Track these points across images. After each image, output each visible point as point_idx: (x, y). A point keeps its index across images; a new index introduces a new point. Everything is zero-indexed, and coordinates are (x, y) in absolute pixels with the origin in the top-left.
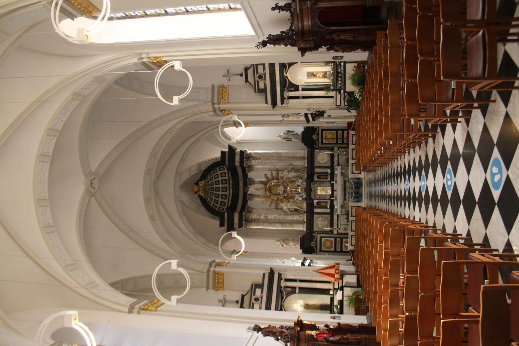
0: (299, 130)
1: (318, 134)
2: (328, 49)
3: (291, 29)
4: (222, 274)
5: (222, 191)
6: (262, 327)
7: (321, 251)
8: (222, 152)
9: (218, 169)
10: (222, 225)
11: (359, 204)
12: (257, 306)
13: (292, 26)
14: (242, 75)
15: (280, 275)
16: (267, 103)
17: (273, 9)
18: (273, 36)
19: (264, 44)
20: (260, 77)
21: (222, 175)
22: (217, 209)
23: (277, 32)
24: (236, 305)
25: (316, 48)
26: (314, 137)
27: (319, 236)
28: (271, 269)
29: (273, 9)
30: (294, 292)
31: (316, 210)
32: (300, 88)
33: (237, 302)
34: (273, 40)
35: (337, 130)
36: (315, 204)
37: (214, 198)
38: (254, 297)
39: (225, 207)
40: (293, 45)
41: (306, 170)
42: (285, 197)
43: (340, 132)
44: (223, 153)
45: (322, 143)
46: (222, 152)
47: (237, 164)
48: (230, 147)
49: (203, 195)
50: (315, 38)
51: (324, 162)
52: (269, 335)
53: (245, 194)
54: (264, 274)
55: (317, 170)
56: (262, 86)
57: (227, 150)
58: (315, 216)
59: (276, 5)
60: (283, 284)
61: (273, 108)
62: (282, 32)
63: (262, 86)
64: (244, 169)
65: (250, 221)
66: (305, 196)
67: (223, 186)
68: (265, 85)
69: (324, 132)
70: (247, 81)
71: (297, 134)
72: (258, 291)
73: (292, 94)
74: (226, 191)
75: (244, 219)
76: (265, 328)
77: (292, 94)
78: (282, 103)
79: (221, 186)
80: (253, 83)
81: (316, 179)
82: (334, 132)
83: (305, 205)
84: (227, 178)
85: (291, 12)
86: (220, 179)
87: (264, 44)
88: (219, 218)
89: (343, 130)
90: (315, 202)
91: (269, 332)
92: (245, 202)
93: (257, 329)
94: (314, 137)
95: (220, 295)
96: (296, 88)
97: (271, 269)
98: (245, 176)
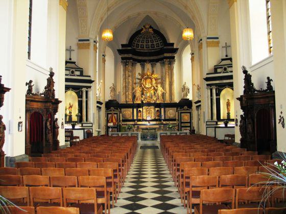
0: (190, 97)
1: (187, 110)
2: (241, 116)
3: (255, 90)
4: (89, 48)
5: (146, 45)
6: (53, 78)
7: (108, 114)
8: (174, 44)
9: (161, 41)
10: (123, 46)
11: (139, 139)
12: (68, 72)
13: (257, 91)
14: (227, 56)
15: (90, 87)
16: (207, 74)
17: (268, 78)
18: (250, 78)
19: (245, 72)
20: (225, 69)
21: (157, 44)
22: (134, 42)
23: (254, 80)
24: (68, 58)
25: (242, 108)
26: (186, 107)
27: (118, 113)
28: (94, 81)
29: (268, 78)
30: (79, 98)
31: (135, 110)
32: (218, 97)
33: (70, 59)
34: (248, 78)
35: (190, 123)
36: (139, 109)
37: (141, 39)
38: (74, 70)
39: (135, 48)
40: (245, 92)
41: (163, 102)
42: (143, 88)
43: (189, 125)
44: (173, 44)
45: (181, 113)
46: (174, 44)
47: (166, 55)
48: (177, 49)
49: (143, 31)
50: (249, 107)
51: (169, 114)
52: (48, 82)
53: (145, 61)
54: (90, 76)
55: (162, 109)
56: (219, 70)
57: (175, 47)
58: (131, 109)
59: (271, 80)
60: (84, 90)
61: (204, 79)
62: (253, 84)
63: (219, 70)
64: (161, 59)
65: (125, 64)
66: (144, 102)
67: (150, 45)
68: (220, 73)
69: (189, 114)
70: (223, 60)
71: (187, 95)
72: (78, 73)
73: (214, 91)
74: (146, 48)
75: (128, 60)
76: (53, 80)
77: (214, 91)
78: (208, 85)
79: (150, 44)
80: (221, 64)
81: (157, 109)
82: (189, 121)
83: (140, 102)
84: (150, 48)
85: (266, 90)
86: (155, 43)
87: (245, 72)
88: (128, 43)
89: (190, 127)
90: (141, 109)
91: (50, 82)
92: (139, 61)
93: (52, 74)
94: (186, 107)
95: (74, 47)
96: (218, 94)
97: (94, 81)
98: (157, 61)
